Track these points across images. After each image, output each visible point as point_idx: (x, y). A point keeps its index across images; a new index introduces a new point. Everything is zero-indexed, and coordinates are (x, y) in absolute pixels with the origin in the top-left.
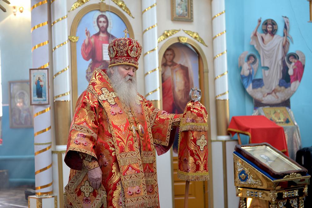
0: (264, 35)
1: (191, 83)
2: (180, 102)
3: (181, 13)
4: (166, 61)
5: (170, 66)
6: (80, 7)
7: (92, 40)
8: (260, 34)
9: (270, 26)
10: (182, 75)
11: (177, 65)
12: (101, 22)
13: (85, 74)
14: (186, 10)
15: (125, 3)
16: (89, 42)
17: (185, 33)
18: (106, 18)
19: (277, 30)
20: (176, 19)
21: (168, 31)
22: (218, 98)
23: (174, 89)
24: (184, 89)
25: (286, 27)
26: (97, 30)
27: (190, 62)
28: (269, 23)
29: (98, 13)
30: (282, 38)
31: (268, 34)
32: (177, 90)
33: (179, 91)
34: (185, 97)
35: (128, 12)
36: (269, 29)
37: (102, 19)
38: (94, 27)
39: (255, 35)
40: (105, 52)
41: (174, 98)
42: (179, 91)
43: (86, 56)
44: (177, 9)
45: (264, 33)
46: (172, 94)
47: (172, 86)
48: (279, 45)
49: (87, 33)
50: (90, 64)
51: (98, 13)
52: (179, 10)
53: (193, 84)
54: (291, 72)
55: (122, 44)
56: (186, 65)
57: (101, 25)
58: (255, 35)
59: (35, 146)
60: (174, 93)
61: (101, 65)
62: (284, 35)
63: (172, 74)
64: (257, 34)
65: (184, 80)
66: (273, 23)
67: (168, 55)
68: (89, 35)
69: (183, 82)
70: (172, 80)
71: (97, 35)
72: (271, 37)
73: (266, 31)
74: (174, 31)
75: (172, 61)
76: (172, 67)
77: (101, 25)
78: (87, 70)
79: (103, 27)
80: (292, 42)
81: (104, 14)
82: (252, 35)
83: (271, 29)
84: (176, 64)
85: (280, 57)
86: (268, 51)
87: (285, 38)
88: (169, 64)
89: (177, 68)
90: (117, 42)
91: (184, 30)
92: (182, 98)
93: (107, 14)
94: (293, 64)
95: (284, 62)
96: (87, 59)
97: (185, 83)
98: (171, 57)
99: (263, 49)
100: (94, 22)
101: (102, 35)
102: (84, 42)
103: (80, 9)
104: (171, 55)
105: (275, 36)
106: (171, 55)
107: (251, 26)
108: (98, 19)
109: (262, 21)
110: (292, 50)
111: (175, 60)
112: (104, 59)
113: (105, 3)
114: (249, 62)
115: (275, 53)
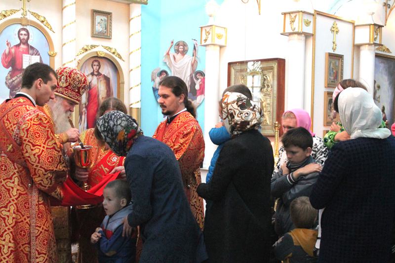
0: (175, 54)
3: (100, 31)
5: (96, 75)
7: (13, 50)
8: (172, 52)
9: (181, 47)
10: (105, 85)
12: (22, 34)
13: (5, 81)
14: (106, 29)
15: (46, 19)
16: (10, 52)
17: (101, 47)
18: (27, 31)
19: (187, 51)
20: (95, 35)
23: (98, 96)
25: (195, 48)
26: (18, 42)
27: (106, 70)
28: (181, 44)
29: (20, 27)
30: (191, 58)
31: (180, 54)
32: (100, 97)
35: (49, 27)
36: (180, 50)
37: (23, 32)
38: (15, 38)
39: (168, 54)
40: (26, 61)
42: (102, 98)
43: (6, 64)
44: (96, 26)
45: (176, 53)
48: (189, 63)
49: (8, 44)
50: (10, 72)
51: (20, 27)
52: (99, 28)
53: (113, 94)
54: (197, 87)
55: (77, 80)
57: (22, 37)
58: (168, 54)
59: (132, 208)
61: (20, 73)
62: (193, 56)
64: (169, 53)
65: (107, 89)
66: (185, 45)
67: (95, 65)
68: (9, 45)
69: (106, 91)
71: (18, 46)
72: (182, 56)
73: (177, 51)
74: (93, 46)
75: (98, 71)
77: (22, 37)
78: (7, 77)
79: (24, 39)
80: (200, 62)
81: (25, 27)
82: (165, 54)
83: (182, 50)
84: (101, 74)
85: (189, 73)
86: (178, 69)
87: (194, 57)
88: (96, 73)
89: (102, 79)
90: (73, 75)
93: (28, 28)
94: (200, 80)
95: (192, 78)
96: (7, 67)
97: (107, 92)
98: (98, 67)
99: (174, 67)
100: (15, 35)
101: (22, 46)
102: (5, 51)
104: (97, 65)
105: (186, 56)
106: (97, 65)
107: (165, 46)
108: (19, 32)
109: (174, 43)
110: (199, 69)
111: (100, 71)
113: (27, 18)
115: (184, 71)
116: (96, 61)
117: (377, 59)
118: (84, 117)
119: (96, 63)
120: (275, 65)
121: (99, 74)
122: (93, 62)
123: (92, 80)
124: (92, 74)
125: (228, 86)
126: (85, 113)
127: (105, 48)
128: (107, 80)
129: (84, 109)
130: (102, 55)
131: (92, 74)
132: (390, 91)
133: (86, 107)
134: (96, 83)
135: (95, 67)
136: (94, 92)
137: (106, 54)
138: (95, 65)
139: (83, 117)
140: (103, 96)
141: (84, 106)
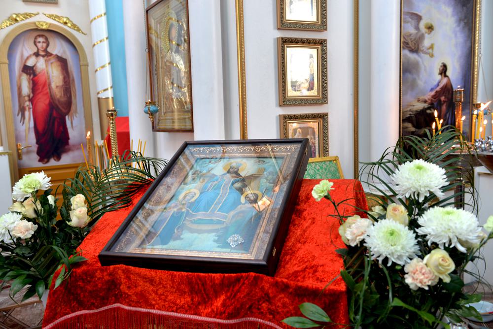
1: (71, 79)
2: (59, 101)
4: (38, 49)
5: (43, 56)
6: (11, 26)
10: (60, 68)
11: (53, 56)
21: (17, 15)
22: (100, 96)
23: (50, 85)
24: (63, 86)
27: (58, 48)
32: (53, 86)
33: (57, 87)
34: (64, 95)
41: (51, 96)
42: (57, 87)
46: (48, 90)
47: (47, 81)
53: (73, 80)
56: (64, 57)
60: (50, 90)
63: (47, 67)
65: (63, 74)
67: (39, 42)
69: (61, 77)
70: (47, 73)
74: (27, 15)
75: (45, 50)
76: (46, 58)
88: (42, 53)
89: (53, 60)
91: (45, 13)
92: (61, 96)
97: (64, 78)
98: (45, 45)
103: (12, 27)
111: (49, 50)
112: (310, 159)
114: (432, 99)
116: (40, 36)
117: (125, 115)
118: (28, 114)
119: (41, 39)
120: (189, 127)
121: (48, 54)
122: (36, 38)
123: (37, 62)
124: (37, 54)
125: (482, 165)
126: (29, 108)
127: (50, 16)
128: (63, 62)
129: (27, 103)
130: (44, 27)
131: (37, 54)
132: (459, 34)
133: (31, 100)
134: (44, 66)
135: (40, 45)
136: (41, 79)
137: (51, 25)
138: (39, 42)
139: (27, 113)
140: (58, 85)
141: (27, 98)
